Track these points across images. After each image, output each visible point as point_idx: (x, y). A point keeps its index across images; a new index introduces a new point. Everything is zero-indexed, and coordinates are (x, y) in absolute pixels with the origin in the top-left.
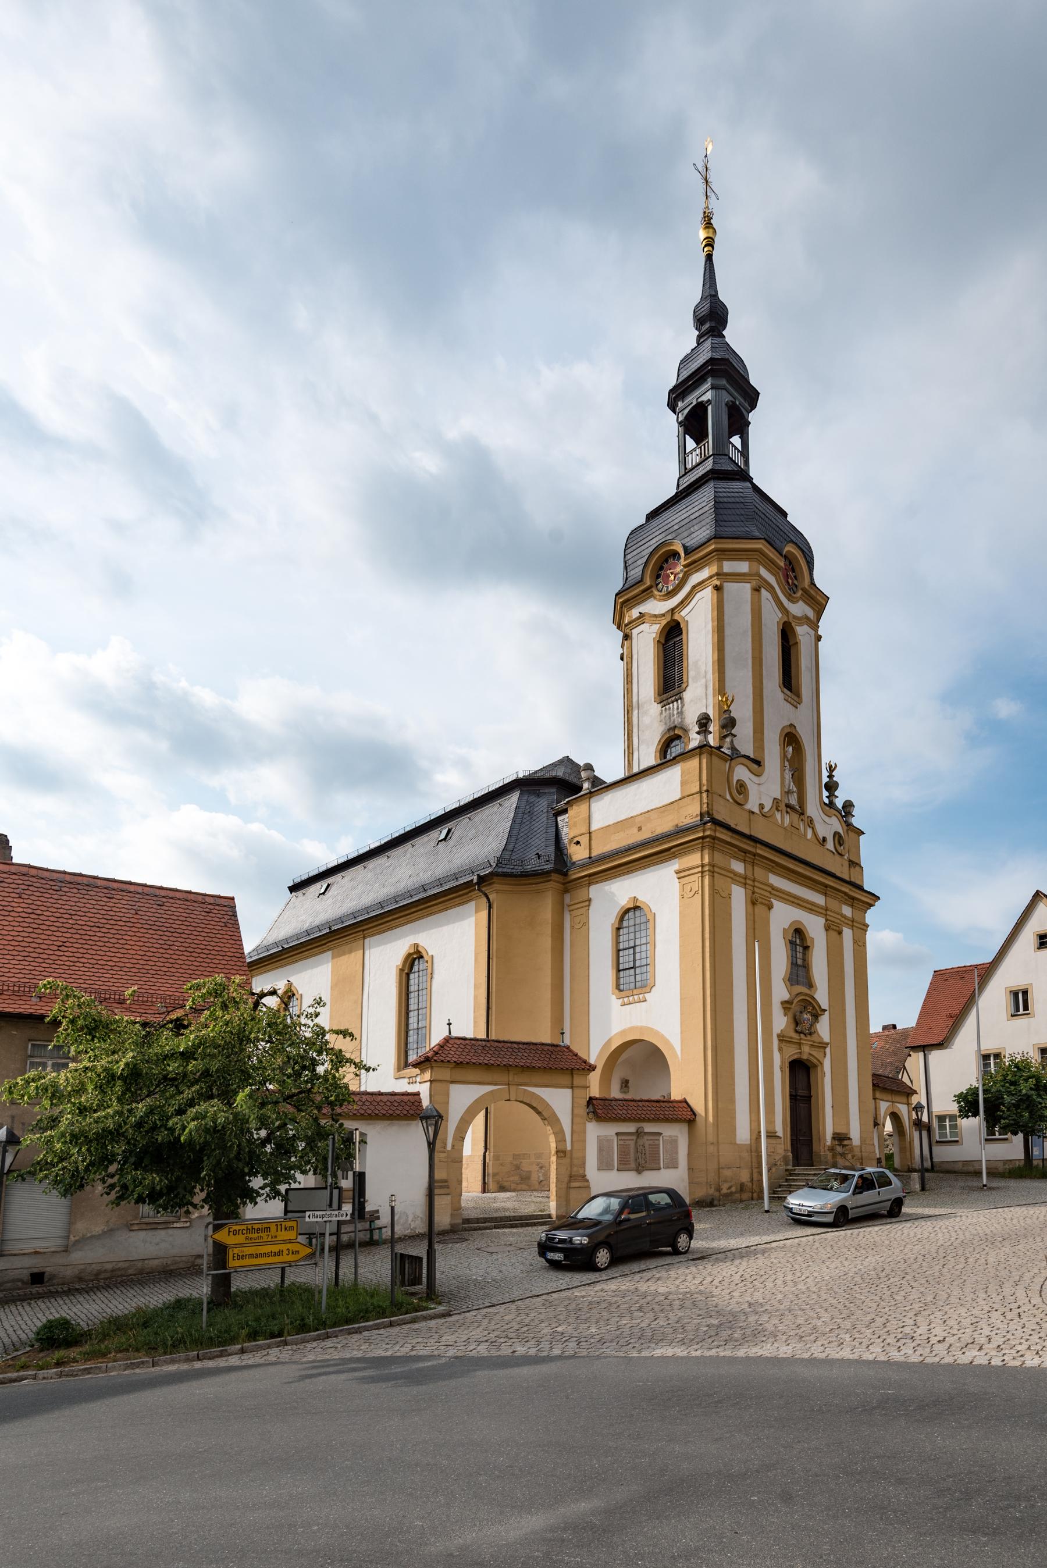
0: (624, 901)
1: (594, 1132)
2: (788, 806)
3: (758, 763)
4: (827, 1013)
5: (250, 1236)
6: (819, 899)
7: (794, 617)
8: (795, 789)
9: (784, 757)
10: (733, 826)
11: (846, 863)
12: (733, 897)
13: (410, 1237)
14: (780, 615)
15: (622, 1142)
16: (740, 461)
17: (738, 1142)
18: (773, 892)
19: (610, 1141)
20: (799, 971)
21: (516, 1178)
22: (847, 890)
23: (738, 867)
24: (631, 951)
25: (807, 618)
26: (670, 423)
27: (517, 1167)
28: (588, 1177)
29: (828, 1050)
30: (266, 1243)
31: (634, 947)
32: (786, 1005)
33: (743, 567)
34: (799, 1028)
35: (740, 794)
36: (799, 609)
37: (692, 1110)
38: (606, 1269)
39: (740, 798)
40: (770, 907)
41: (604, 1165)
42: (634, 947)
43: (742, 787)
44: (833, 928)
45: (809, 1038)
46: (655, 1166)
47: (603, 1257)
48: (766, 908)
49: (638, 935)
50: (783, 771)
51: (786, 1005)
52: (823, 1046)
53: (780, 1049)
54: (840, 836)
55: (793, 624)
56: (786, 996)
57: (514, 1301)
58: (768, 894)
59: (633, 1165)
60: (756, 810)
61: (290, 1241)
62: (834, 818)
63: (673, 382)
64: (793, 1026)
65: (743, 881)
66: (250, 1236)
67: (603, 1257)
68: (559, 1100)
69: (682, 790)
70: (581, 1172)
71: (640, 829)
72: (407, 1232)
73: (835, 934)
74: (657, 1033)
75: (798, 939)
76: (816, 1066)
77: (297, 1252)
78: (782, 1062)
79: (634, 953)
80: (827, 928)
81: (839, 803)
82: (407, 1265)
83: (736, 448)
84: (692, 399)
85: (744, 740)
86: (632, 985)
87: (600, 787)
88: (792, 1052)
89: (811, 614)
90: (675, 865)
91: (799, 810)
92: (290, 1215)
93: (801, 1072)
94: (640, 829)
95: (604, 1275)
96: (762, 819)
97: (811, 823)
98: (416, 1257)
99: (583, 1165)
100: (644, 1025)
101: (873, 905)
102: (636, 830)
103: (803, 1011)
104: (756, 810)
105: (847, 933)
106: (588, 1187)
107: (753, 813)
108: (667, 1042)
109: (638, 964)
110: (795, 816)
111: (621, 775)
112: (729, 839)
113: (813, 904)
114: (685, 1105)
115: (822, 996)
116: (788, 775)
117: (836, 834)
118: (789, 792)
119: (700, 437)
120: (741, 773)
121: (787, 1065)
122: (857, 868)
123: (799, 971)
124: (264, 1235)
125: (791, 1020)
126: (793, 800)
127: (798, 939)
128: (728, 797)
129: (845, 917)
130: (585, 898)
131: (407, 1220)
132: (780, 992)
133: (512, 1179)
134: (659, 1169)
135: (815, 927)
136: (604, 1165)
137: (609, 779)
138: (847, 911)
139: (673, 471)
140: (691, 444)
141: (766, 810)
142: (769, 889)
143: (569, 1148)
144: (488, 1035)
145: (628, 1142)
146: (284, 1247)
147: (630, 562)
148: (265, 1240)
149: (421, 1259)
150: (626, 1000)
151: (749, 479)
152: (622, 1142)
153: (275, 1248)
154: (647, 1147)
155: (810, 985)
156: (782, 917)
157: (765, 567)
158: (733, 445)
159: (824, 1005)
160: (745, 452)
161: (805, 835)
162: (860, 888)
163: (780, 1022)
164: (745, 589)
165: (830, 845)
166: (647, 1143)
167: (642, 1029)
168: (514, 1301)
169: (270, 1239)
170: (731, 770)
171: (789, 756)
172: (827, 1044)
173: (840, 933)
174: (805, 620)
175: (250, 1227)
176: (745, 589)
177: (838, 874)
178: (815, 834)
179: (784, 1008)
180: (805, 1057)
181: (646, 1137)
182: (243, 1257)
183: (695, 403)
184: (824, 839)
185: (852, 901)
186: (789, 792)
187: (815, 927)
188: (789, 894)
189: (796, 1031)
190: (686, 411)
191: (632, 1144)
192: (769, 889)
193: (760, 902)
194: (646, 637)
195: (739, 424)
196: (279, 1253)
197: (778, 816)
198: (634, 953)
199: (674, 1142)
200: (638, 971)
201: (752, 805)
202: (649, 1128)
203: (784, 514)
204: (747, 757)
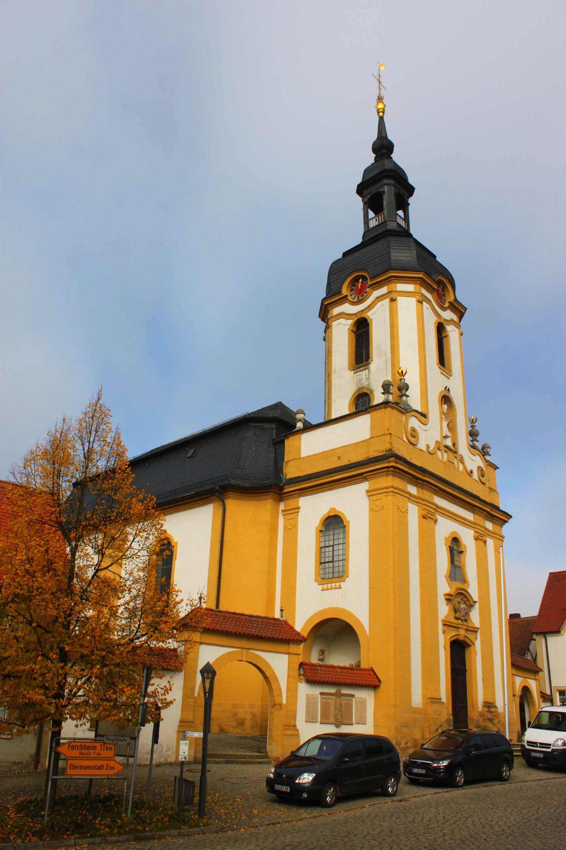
0: (324, 512)
1: (305, 690)
2: (446, 447)
3: (424, 416)
4: (477, 604)
5: (83, 751)
6: (470, 516)
7: (445, 320)
8: (450, 435)
9: (442, 413)
10: (408, 460)
11: (487, 490)
12: (409, 512)
13: (165, 764)
14: (436, 318)
15: (324, 700)
16: (403, 223)
17: (413, 705)
18: (438, 509)
19: (315, 699)
20: (456, 571)
21: (234, 723)
22: (489, 510)
23: (413, 490)
24: (331, 548)
25: (452, 320)
26: (358, 202)
27: (235, 715)
28: (298, 727)
29: (479, 635)
30: (94, 759)
31: (333, 546)
32: (449, 599)
33: (410, 287)
34: (457, 615)
35: (413, 437)
36: (448, 315)
37: (378, 678)
38: (461, 786)
39: (413, 440)
40: (436, 521)
41: (310, 719)
42: (333, 546)
43: (414, 433)
44: (480, 538)
45: (465, 623)
46: (348, 722)
47: (460, 777)
48: (433, 522)
49: (336, 537)
50: (441, 421)
51: (449, 599)
52: (475, 631)
53: (444, 632)
54: (482, 470)
55: (444, 324)
56: (448, 590)
57: (549, 779)
58: (434, 511)
59: (332, 720)
60: (424, 449)
61: (110, 759)
62: (477, 456)
63: (360, 180)
64: (453, 613)
65: (416, 500)
66: (83, 751)
67: (460, 777)
68: (279, 663)
69: (371, 434)
70: (293, 723)
71: (339, 458)
72: (162, 760)
73: (482, 543)
74: (350, 613)
75: (455, 547)
76: (468, 646)
77: (113, 768)
78: (445, 641)
79: (333, 551)
80: (476, 539)
81: (479, 445)
82: (184, 786)
83: (401, 218)
84: (373, 190)
85: (414, 399)
86: (331, 576)
87: (309, 427)
88: (452, 633)
89: (455, 318)
90: (364, 486)
91: (452, 450)
92: (98, 738)
93: (459, 650)
94: (339, 458)
95: (332, 810)
96: (428, 455)
97: (462, 461)
98: (191, 782)
99: (294, 717)
100: (340, 606)
101: (507, 522)
102: (337, 459)
103: (460, 600)
104: (424, 449)
105: (490, 542)
106: (298, 735)
107: (422, 450)
108: (359, 622)
109: (336, 559)
110: (451, 454)
111: (323, 421)
112: (406, 470)
113: (465, 519)
114: (372, 672)
115: (473, 591)
116: (445, 424)
117: (479, 468)
118: (446, 437)
119: (378, 210)
120: (414, 422)
121: (449, 644)
122: (495, 493)
123: (456, 571)
124: (92, 752)
125: (452, 609)
126: (449, 442)
127: (455, 547)
128: (405, 439)
129: (488, 530)
130: (295, 506)
131: (162, 750)
132: (444, 587)
133: (230, 723)
134: (352, 724)
135: (467, 537)
136: (310, 719)
137: (314, 423)
138: (489, 525)
139: (361, 230)
140: (371, 214)
141: (431, 449)
142: (435, 507)
143: (284, 702)
144: (218, 606)
145: (328, 700)
146: (104, 763)
147: (332, 284)
148: (92, 755)
149: (193, 783)
150: (325, 586)
151: (411, 236)
152: (324, 700)
153: (99, 763)
154: (343, 706)
155: (464, 581)
156: (445, 528)
157: (425, 289)
158: (399, 216)
159: (475, 597)
160: (406, 218)
161: (459, 468)
162: (497, 508)
163: (444, 610)
164: (412, 301)
165: (475, 475)
166: (343, 702)
167: (331, 609)
168: (549, 779)
169: (96, 756)
170: (407, 420)
171: (445, 411)
172: (478, 629)
173: (485, 542)
174: (452, 322)
175: (83, 744)
176: (412, 301)
177: (482, 498)
178: (465, 468)
179: (446, 599)
180: (461, 638)
181: (342, 698)
182: (76, 767)
183: (374, 192)
184: (471, 472)
185: (491, 517)
186: (446, 437)
187: (467, 537)
188: (448, 511)
189: (456, 618)
190: (368, 197)
191: (332, 702)
192: (435, 507)
193: (429, 516)
194: (342, 331)
195: (403, 204)
196: (100, 768)
197: (439, 453)
198: (333, 551)
199: (363, 703)
200: (336, 564)
201: (422, 445)
202: (345, 691)
203: (434, 257)
204: (415, 411)
